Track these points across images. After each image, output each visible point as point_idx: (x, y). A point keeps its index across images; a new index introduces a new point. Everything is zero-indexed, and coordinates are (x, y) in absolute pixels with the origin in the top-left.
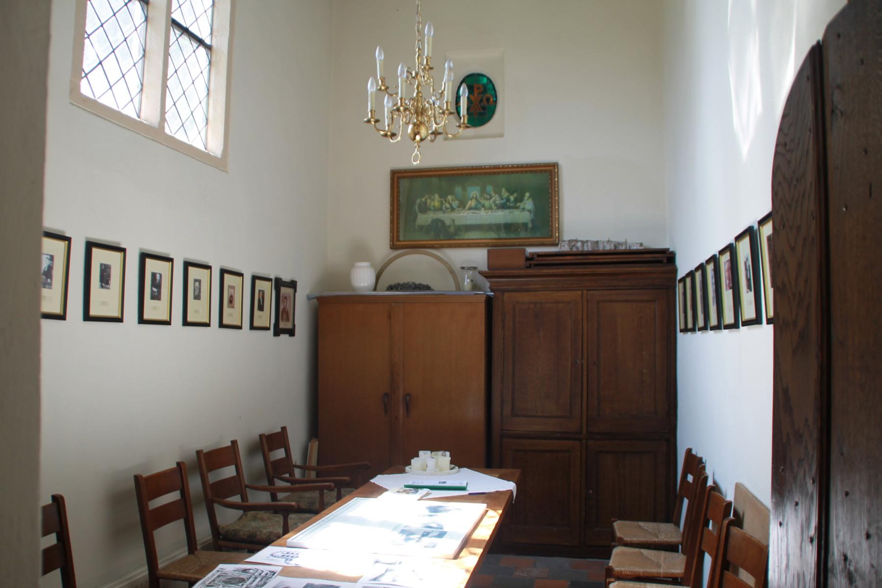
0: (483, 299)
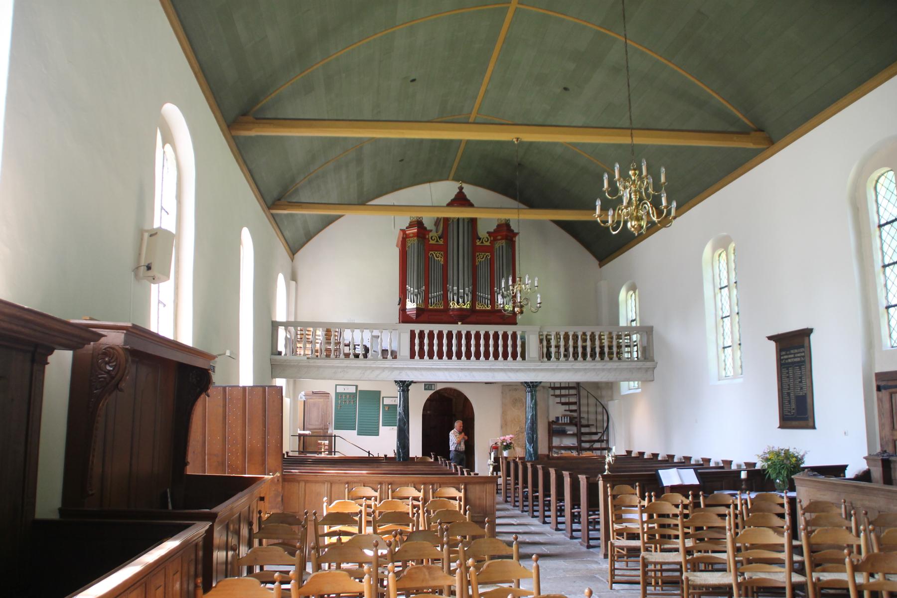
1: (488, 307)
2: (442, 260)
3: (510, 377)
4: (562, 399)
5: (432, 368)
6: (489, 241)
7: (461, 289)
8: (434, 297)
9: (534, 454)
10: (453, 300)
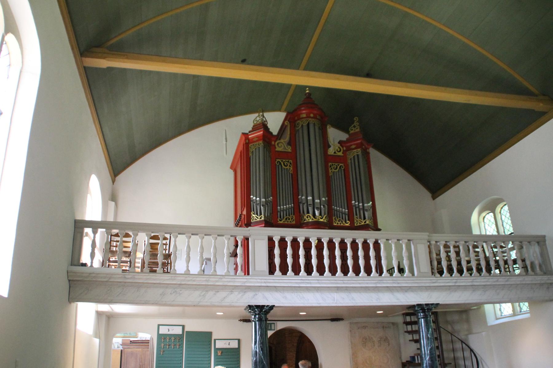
0: (120, 350)
1: (346, 222)
2: (291, 169)
3: (398, 299)
4: (414, 335)
5: (299, 287)
6: (342, 151)
7: (317, 202)
8: (283, 211)
10: (308, 212)
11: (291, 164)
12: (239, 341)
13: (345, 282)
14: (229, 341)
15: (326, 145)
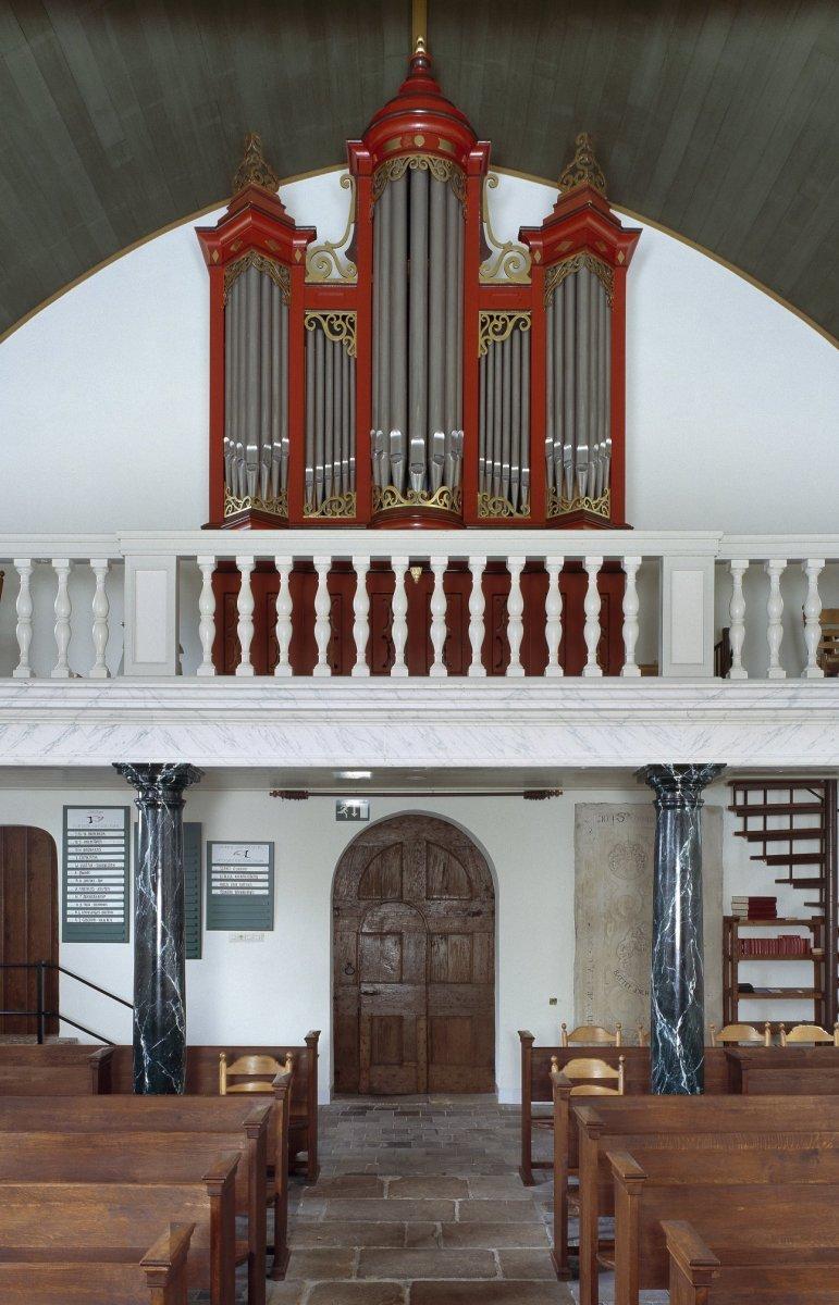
1: (519, 511)
2: (354, 341)
7: (417, 446)
9: (686, 1057)
11: (352, 324)
12: (272, 845)
13: (401, 694)
14: (244, 848)
15: (476, 247)
